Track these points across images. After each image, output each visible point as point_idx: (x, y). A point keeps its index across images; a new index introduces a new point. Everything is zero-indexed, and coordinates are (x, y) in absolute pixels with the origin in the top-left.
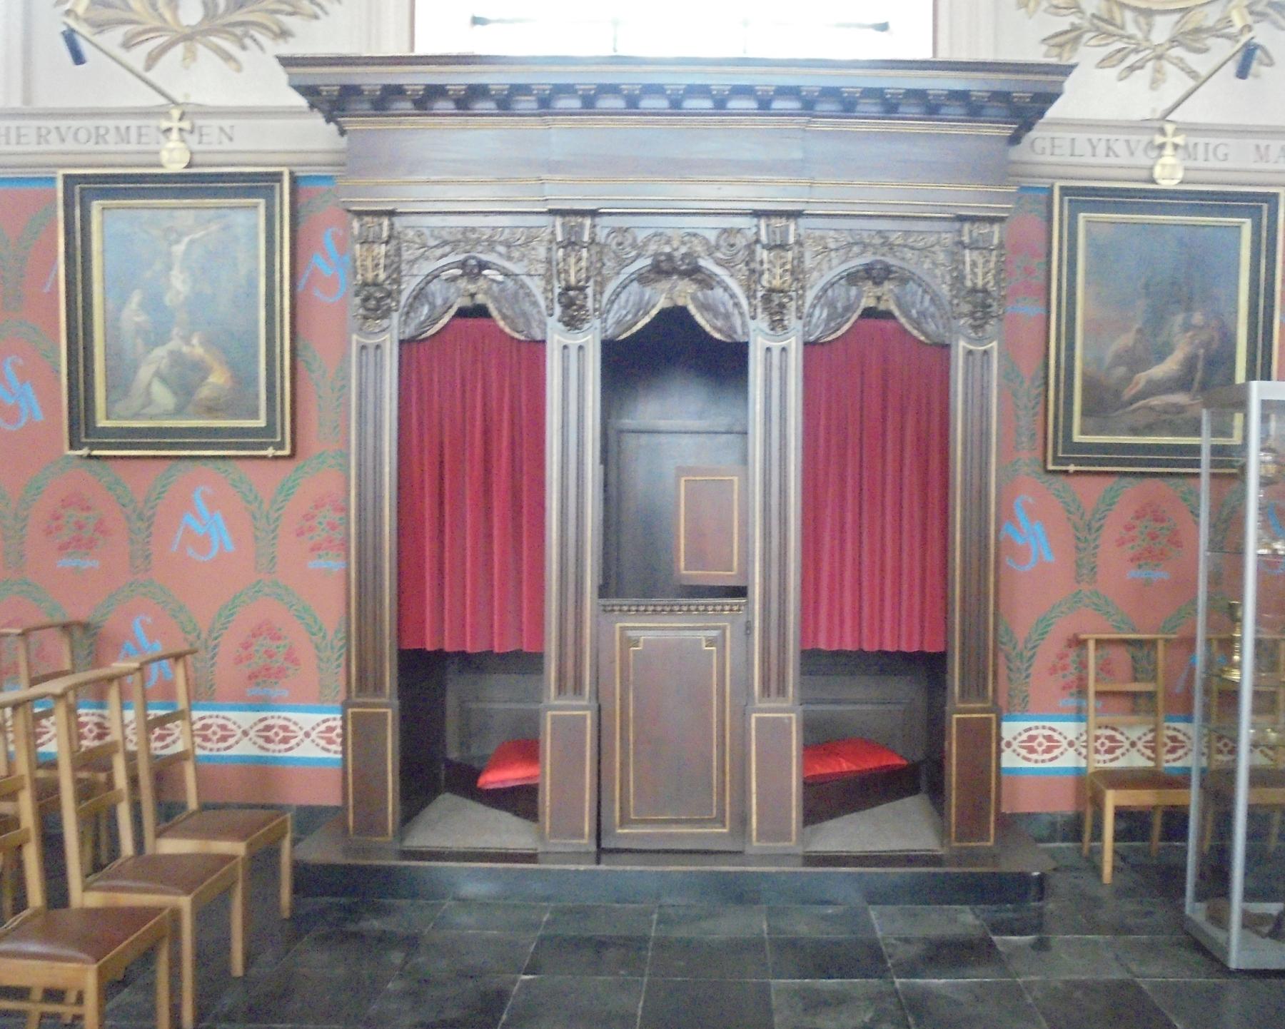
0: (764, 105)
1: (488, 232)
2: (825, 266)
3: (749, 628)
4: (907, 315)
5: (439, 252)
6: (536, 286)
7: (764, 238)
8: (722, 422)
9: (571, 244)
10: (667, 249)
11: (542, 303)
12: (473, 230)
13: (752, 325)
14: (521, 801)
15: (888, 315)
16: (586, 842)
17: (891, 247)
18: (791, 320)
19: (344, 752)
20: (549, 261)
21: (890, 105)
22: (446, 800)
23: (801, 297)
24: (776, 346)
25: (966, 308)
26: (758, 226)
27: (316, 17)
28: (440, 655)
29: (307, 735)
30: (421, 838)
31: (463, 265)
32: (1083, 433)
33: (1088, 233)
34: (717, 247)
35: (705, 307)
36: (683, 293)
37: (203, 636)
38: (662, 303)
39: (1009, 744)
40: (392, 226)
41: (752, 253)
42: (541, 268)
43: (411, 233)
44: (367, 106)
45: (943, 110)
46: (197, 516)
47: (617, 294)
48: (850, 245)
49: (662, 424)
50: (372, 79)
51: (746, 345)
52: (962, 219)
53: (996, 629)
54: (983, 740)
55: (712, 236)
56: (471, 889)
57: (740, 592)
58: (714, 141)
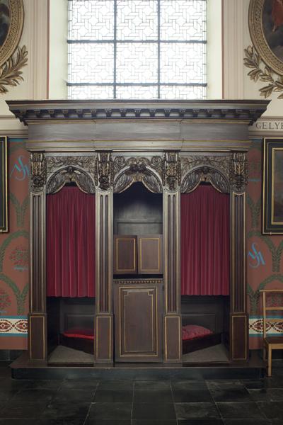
0: (167, 115)
1: (76, 158)
2: (188, 168)
3: (164, 288)
4: (215, 183)
5: (59, 165)
6: (91, 175)
7: (167, 159)
8: (153, 219)
9: (103, 161)
10: (135, 163)
11: (93, 181)
12: (71, 157)
13: (164, 188)
14: (87, 346)
15: (209, 184)
16: (110, 360)
17: (210, 161)
18: (178, 187)
19: (28, 331)
20: (96, 167)
21: (209, 114)
22: (60, 348)
23: (180, 178)
24: (172, 195)
25: (235, 181)
26: (165, 155)
27: (16, 85)
28: (60, 297)
29: (13, 326)
30: (53, 360)
31: (67, 169)
32: (274, 221)
33: (275, 154)
34: (152, 162)
35: (147, 182)
36: (141, 177)
37: (21, 292)
38: (134, 181)
39: (251, 326)
40: (43, 157)
41: (164, 164)
42: (93, 170)
43: (50, 158)
44: (35, 116)
45: (227, 116)
46: (253, 253)
47: (118, 178)
48: (196, 161)
49: (132, 220)
50: (37, 108)
51: (162, 194)
52: (233, 152)
53: (246, 288)
54: (243, 325)
55: (150, 159)
56: (71, 376)
57: (161, 276)
58: (148, 128)
